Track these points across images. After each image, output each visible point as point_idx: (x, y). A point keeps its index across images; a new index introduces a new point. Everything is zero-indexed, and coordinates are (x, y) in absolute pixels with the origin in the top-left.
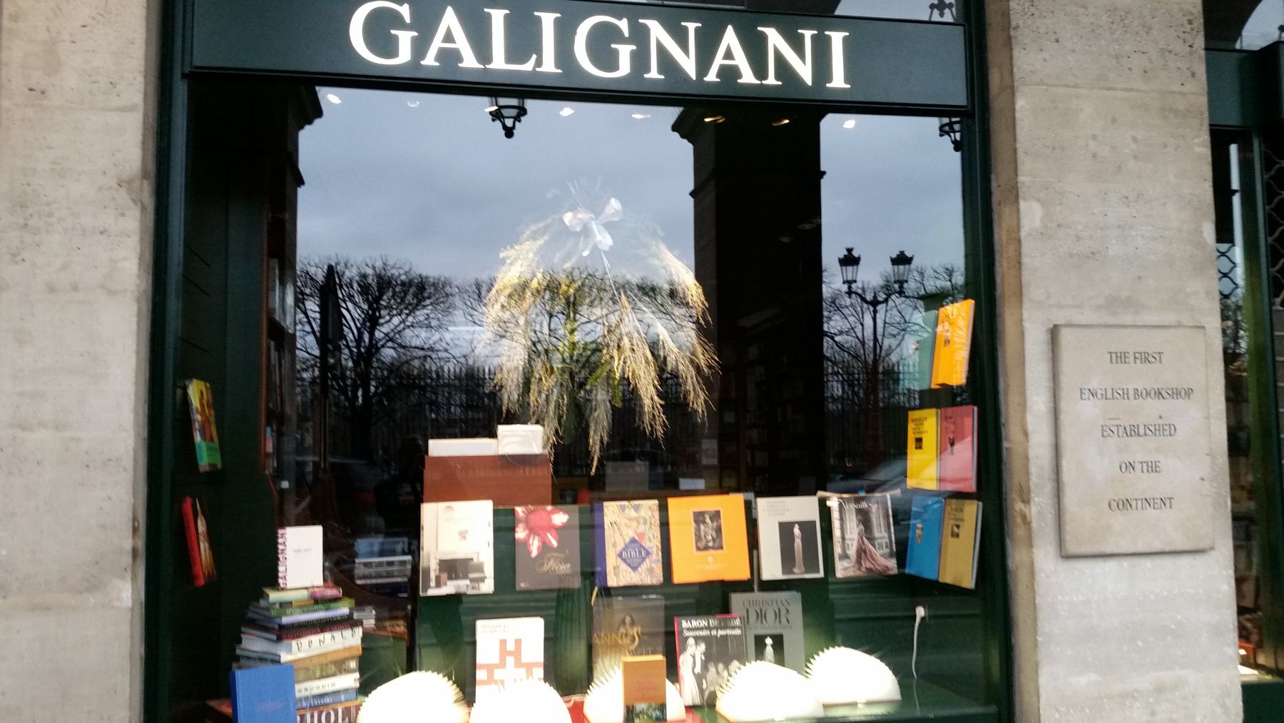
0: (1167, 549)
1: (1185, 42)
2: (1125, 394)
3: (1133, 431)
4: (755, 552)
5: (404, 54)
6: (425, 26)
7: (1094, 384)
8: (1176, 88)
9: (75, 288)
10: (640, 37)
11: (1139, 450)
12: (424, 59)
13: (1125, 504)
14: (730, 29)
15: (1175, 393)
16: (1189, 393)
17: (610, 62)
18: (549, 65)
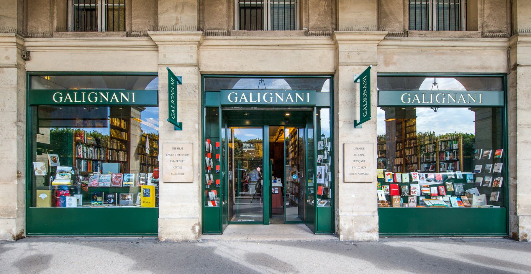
0: (183, 182)
2: (175, 155)
3: (177, 161)
5: (236, 101)
6: (64, 96)
7: (169, 153)
8: (191, 99)
9: (8, 138)
10: (99, 95)
11: (177, 164)
13: (174, 174)
15: (185, 155)
16: (188, 155)
17: (94, 100)
18: (259, 101)
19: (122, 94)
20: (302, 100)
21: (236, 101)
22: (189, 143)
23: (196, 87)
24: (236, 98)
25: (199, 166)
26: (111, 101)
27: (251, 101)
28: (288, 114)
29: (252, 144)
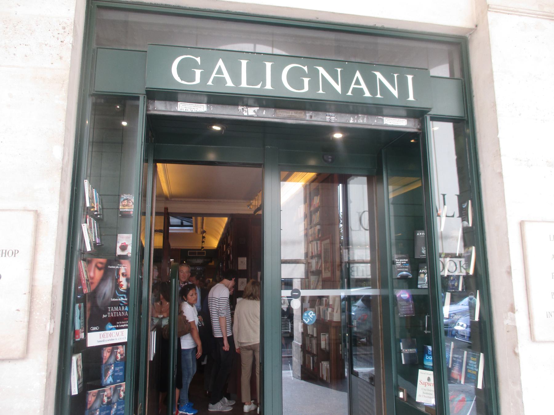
1: (58, 39)
4: (395, 308)
5: (198, 80)
10: (314, 75)
12: (266, 86)
14: (221, 60)
16: (15, 253)
18: (268, 86)
19: (379, 75)
20: (395, 93)
21: (198, 80)
22: (25, 210)
23: (67, 29)
24: (198, 72)
25: (53, 293)
26: (350, 93)
27: (244, 84)
28: (216, 128)
29: (187, 219)
